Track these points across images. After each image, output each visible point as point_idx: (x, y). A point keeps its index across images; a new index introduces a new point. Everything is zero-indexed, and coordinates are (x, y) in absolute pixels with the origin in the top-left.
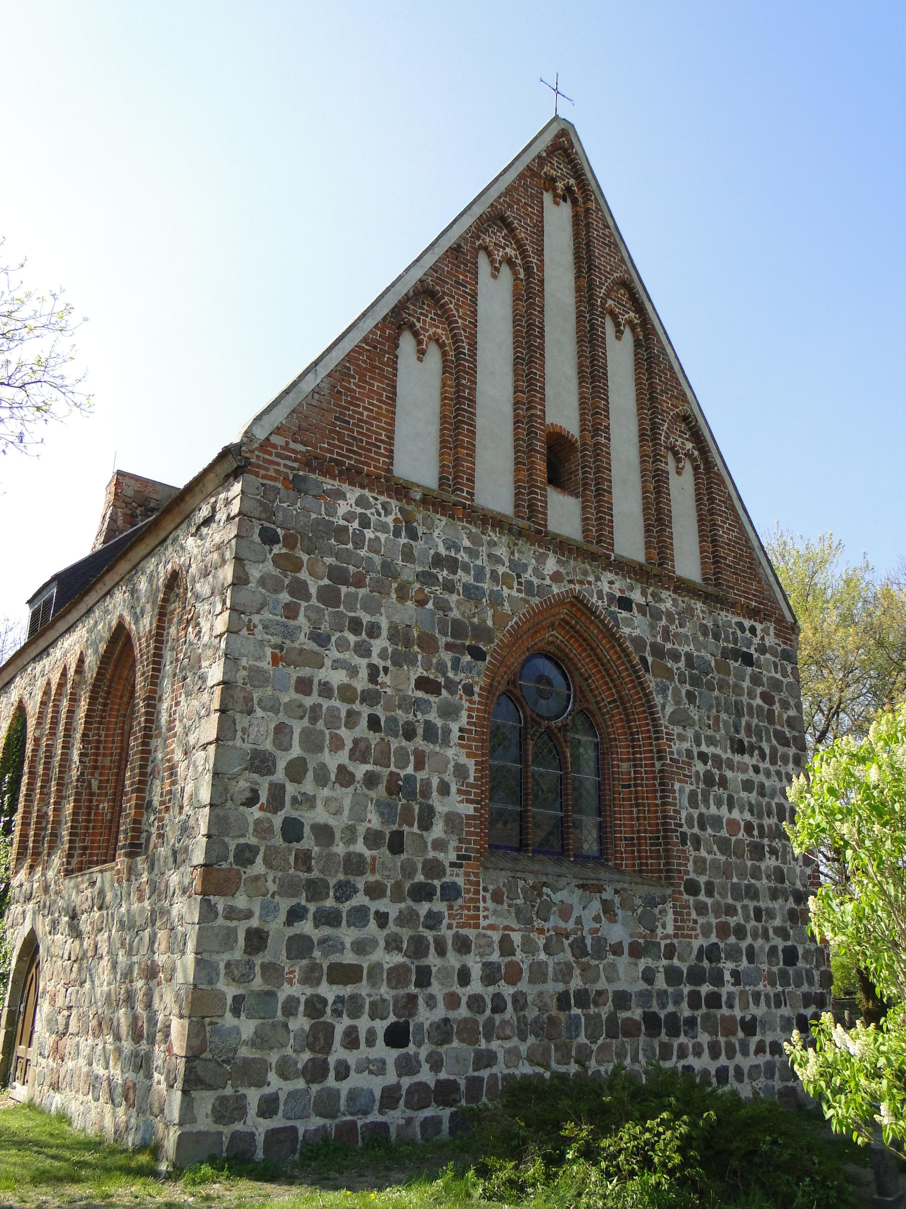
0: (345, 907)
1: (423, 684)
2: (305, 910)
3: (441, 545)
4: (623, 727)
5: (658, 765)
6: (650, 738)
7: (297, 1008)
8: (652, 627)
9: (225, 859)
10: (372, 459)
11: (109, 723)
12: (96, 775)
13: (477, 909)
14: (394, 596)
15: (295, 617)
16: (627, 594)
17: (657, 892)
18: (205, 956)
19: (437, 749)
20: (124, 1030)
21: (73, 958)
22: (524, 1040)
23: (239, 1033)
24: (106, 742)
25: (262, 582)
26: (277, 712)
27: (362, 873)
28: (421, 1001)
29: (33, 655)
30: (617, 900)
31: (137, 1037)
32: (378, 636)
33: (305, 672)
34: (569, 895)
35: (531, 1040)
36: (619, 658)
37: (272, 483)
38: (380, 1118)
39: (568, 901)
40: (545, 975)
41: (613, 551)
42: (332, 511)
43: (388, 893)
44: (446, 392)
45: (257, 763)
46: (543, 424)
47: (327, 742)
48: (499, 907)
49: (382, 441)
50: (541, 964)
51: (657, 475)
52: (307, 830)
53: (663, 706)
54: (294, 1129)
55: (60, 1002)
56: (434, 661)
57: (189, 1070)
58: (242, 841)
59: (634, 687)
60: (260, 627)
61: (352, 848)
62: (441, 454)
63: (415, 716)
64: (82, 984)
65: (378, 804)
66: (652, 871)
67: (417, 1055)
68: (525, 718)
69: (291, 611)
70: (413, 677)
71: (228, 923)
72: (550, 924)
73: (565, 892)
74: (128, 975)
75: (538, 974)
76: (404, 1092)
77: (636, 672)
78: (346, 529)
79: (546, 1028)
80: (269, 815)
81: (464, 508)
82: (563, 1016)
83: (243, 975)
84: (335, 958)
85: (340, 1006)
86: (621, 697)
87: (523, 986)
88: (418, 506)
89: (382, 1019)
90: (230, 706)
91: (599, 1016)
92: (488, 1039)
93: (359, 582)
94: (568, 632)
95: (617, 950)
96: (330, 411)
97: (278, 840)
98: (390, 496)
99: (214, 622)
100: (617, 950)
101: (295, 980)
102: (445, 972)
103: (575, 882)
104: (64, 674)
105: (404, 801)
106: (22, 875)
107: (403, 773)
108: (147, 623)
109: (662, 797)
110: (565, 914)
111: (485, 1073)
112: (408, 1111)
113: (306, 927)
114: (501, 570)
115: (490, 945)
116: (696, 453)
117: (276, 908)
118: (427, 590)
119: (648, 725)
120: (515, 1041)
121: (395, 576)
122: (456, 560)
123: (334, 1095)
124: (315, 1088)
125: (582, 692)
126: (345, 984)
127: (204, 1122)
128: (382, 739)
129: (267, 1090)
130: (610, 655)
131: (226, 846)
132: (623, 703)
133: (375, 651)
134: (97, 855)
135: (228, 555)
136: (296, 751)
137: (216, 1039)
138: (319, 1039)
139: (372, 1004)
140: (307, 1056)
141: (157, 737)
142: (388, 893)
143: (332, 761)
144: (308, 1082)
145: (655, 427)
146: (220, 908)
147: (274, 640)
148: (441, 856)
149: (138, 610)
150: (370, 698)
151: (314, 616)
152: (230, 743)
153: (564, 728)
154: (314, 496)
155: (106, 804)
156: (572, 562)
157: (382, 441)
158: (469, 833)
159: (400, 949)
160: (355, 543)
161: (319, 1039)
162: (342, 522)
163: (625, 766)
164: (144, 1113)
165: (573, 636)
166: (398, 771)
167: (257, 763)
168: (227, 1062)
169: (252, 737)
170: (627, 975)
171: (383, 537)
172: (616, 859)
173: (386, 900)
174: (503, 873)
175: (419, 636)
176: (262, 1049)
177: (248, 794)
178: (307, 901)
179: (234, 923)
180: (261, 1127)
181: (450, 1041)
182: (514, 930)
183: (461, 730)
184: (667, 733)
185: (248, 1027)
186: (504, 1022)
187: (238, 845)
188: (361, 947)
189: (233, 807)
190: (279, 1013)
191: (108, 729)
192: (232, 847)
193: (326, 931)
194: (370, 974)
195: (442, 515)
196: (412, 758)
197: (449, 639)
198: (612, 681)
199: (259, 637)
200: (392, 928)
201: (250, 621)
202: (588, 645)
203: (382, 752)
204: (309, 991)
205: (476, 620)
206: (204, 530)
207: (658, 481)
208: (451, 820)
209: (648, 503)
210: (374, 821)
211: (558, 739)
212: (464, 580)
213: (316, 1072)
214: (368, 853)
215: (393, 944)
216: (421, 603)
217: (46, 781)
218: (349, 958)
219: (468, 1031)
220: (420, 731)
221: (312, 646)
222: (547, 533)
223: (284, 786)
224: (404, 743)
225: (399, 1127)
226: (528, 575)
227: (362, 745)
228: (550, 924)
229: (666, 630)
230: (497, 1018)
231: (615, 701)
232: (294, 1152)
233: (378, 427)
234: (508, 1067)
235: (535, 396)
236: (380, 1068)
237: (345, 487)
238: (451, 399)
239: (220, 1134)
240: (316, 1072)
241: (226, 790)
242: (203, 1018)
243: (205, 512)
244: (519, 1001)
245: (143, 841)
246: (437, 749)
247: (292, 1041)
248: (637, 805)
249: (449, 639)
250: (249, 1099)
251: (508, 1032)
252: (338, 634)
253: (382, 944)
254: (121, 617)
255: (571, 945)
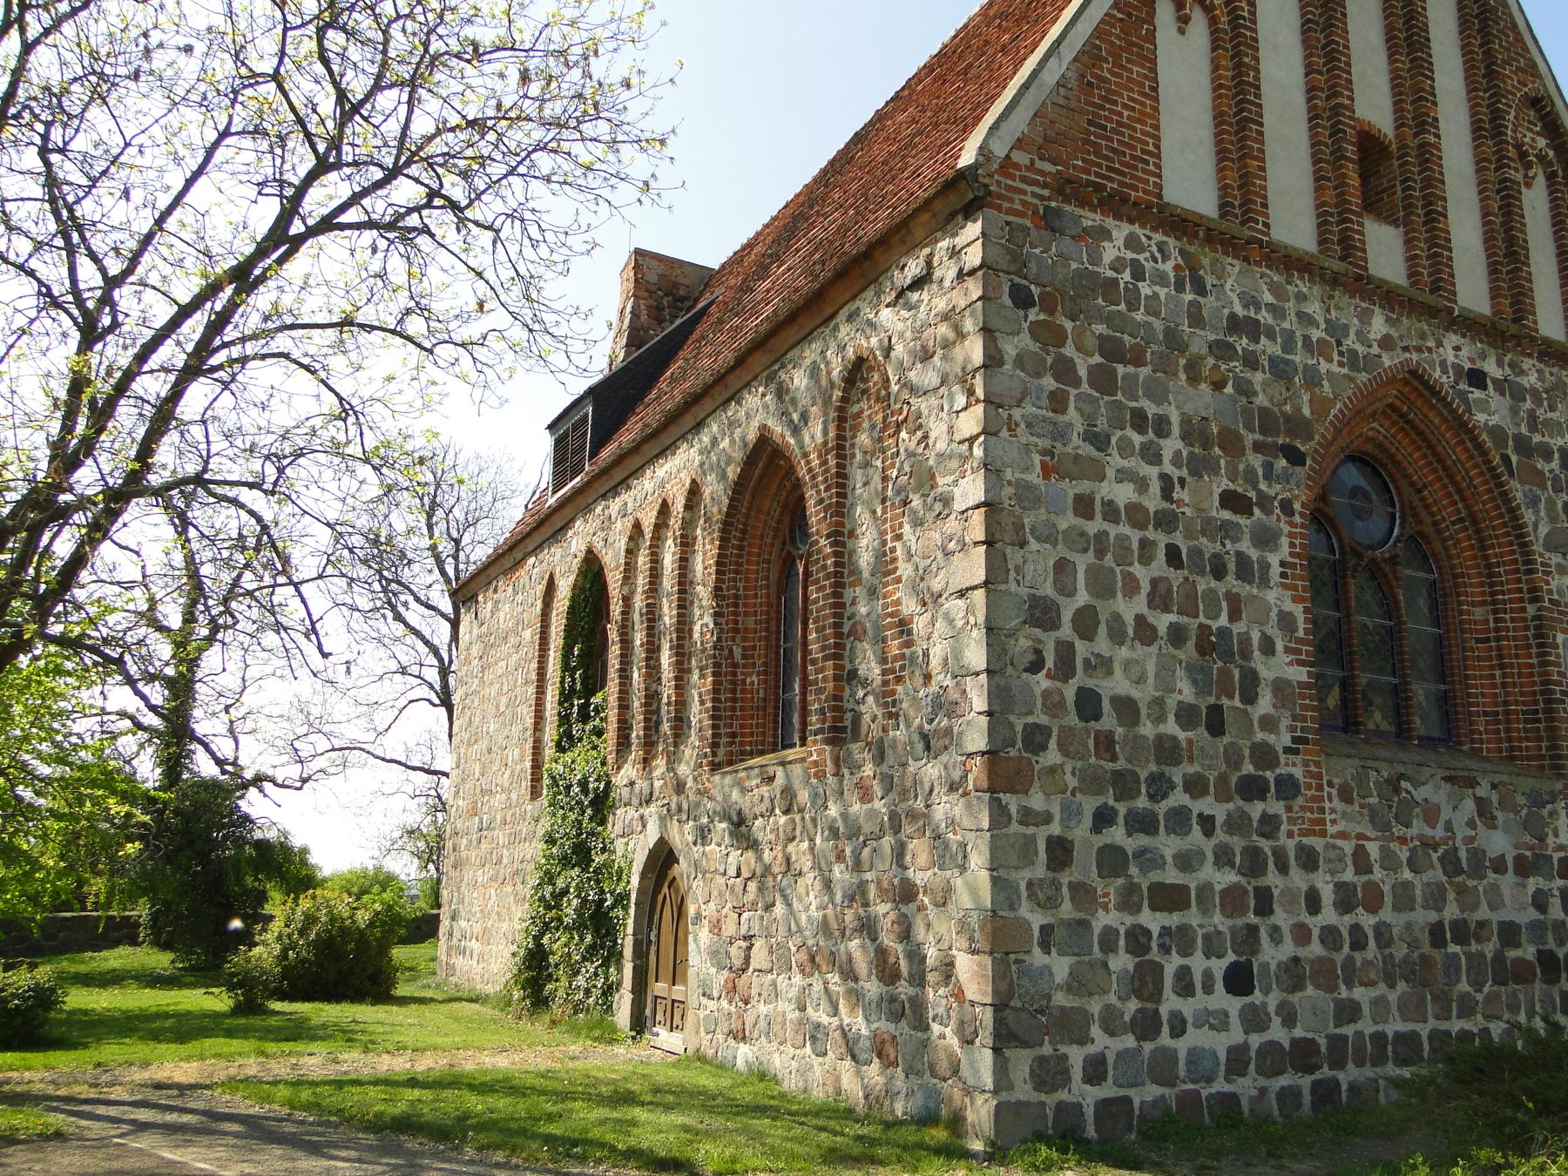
0: (1163, 807)
1: (1230, 500)
2: (1114, 812)
3: (1236, 301)
4: (1474, 557)
5: (1531, 610)
6: (1517, 571)
7: (1116, 942)
8: (1514, 411)
9: (1013, 744)
10: (1139, 179)
11: (748, 571)
12: (738, 640)
13: (1322, 810)
14: (1183, 376)
15: (1064, 411)
16: (1478, 365)
17: (1544, 786)
18: (1003, 873)
19: (1255, 591)
20: (862, 965)
21: (745, 874)
22: (1392, 986)
23: (1051, 974)
24: (746, 597)
25: (1020, 361)
26: (1055, 544)
27: (1177, 763)
28: (1263, 934)
29: (602, 491)
30: (1495, 797)
31: (888, 974)
32: (1168, 435)
33: (1084, 487)
34: (1432, 791)
35: (1402, 986)
36: (1471, 457)
37: (1019, 221)
38: (1227, 1088)
39: (1434, 799)
40: (1413, 900)
41: (1455, 302)
42: (1095, 259)
43: (1212, 789)
44: (1220, 77)
45: (1038, 614)
46: (1352, 119)
47: (1120, 584)
48: (1349, 808)
49: (1150, 153)
50: (1407, 885)
51: (1506, 188)
52: (1106, 705)
53: (1536, 525)
54: (1127, 1100)
55: (729, 929)
56: (1241, 467)
57: (999, 1022)
58: (1030, 719)
59: (1493, 499)
60: (1023, 426)
61: (1162, 729)
62: (1220, 170)
63: (1223, 545)
64: (769, 907)
65: (1189, 668)
66: (1529, 758)
67: (1264, 1004)
68: (1342, 547)
69: (1058, 402)
70: (1217, 491)
71: (1023, 830)
72: (1413, 831)
73: (1426, 787)
74: (857, 895)
75: (1404, 898)
76: (1253, 1054)
77: (1498, 476)
78: (1115, 282)
79: (1416, 972)
80: (1059, 684)
81: (1261, 247)
82: (1437, 955)
83: (1049, 898)
84: (1155, 876)
85: (1167, 940)
86: (1472, 515)
87: (1387, 914)
88: (1202, 246)
89: (1219, 957)
90: (998, 537)
91: (1482, 955)
92: (1350, 987)
93: (1138, 361)
94: (1394, 423)
95: (1499, 866)
96: (1082, 112)
97: (1072, 719)
98: (1166, 234)
99: (954, 423)
100: (1499, 866)
101: (1111, 906)
102: (1290, 895)
103: (1441, 773)
104: (664, 509)
105: (1220, 664)
106: (629, 771)
107: (1215, 625)
108: (816, 432)
109: (1538, 655)
110: (1431, 816)
111: (1348, 1030)
112: (1260, 1078)
113: (1117, 834)
114: (1316, 334)
115: (1341, 859)
116: (1551, 153)
117: (1080, 812)
118: (1224, 367)
119: (1513, 552)
120: (1381, 989)
121: (1183, 348)
122: (1257, 321)
123: (1170, 1056)
124: (1148, 1047)
125: (1412, 508)
126: (1171, 911)
127: (1023, 1091)
128: (1186, 579)
129: (1091, 1049)
130: (1456, 454)
131: (1011, 726)
132: (1475, 522)
133: (1167, 456)
134: (750, 743)
135: (969, 325)
136: (1082, 597)
137: (1025, 982)
138: (1146, 982)
139: (1206, 937)
140: (1133, 1005)
141: (852, 585)
142: (1212, 789)
143: (1130, 609)
144: (1138, 1039)
145: (1497, 116)
146: (1013, 809)
147: (1043, 443)
148: (1271, 739)
149: (795, 417)
150: (1166, 521)
151: (1086, 408)
152: (1003, 587)
153: (1393, 560)
154: (1073, 237)
155: (755, 678)
156: (1405, 320)
157: (1150, 153)
158: (1305, 708)
159: (1232, 865)
160: (1128, 303)
161: (1146, 982)
162: (1110, 274)
163: (1479, 613)
164: (919, 1074)
165: (1402, 429)
166: (1209, 622)
167: (1038, 614)
168: (1041, 1011)
169: (1028, 578)
170: (1512, 900)
171: (1162, 292)
172: (1473, 741)
173: (1210, 799)
174: (1350, 761)
175: (1219, 433)
176: (1081, 996)
177: (1032, 657)
178: (1116, 800)
179: (1031, 830)
180: (1090, 1096)
181: (1303, 988)
182: (1370, 839)
183: (1283, 564)
184: (1543, 564)
185: (1061, 966)
186: (1367, 963)
187: (1026, 726)
188: (1186, 862)
189: (1015, 674)
190: (1096, 948)
191: (747, 580)
192: (1019, 729)
193: (1142, 840)
194: (1198, 896)
195: (1234, 257)
196: (1224, 604)
197: (1258, 437)
198: (1459, 491)
199: (1023, 440)
200: (1221, 836)
201: (1010, 416)
202: (1425, 440)
203: (1187, 596)
204: (1129, 920)
205: (1288, 408)
206: (914, 296)
207: (1508, 196)
208: (1280, 686)
209: (1492, 231)
210: (1186, 691)
211: (1385, 576)
212: (1269, 351)
213: (1146, 1026)
214: (1182, 735)
215: (1223, 857)
216: (1218, 386)
217: (652, 650)
218: (1172, 876)
219: (1324, 975)
220: (1232, 567)
221: (1088, 450)
222: (1370, 279)
223: (1073, 644)
224: (1213, 584)
225: (1252, 1099)
226: (1350, 342)
227: (1162, 587)
228: (1413, 831)
229: (1532, 415)
230: (1357, 955)
231: (1462, 520)
232: (1130, 1128)
233: (1143, 133)
234: (1376, 1023)
235: (1340, 77)
236: (1219, 1021)
237: (1110, 222)
238: (1228, 88)
239: (1043, 1104)
240: (1146, 1026)
241: (1004, 651)
242: (1007, 954)
243: (914, 268)
244: (1382, 932)
245: (848, 723)
246: (1255, 591)
247: (1115, 986)
248: (1502, 666)
249: (1258, 437)
250: (1071, 1060)
251: (1373, 976)
252: (1119, 433)
253: (1210, 858)
254: (763, 428)
255: (1441, 859)
